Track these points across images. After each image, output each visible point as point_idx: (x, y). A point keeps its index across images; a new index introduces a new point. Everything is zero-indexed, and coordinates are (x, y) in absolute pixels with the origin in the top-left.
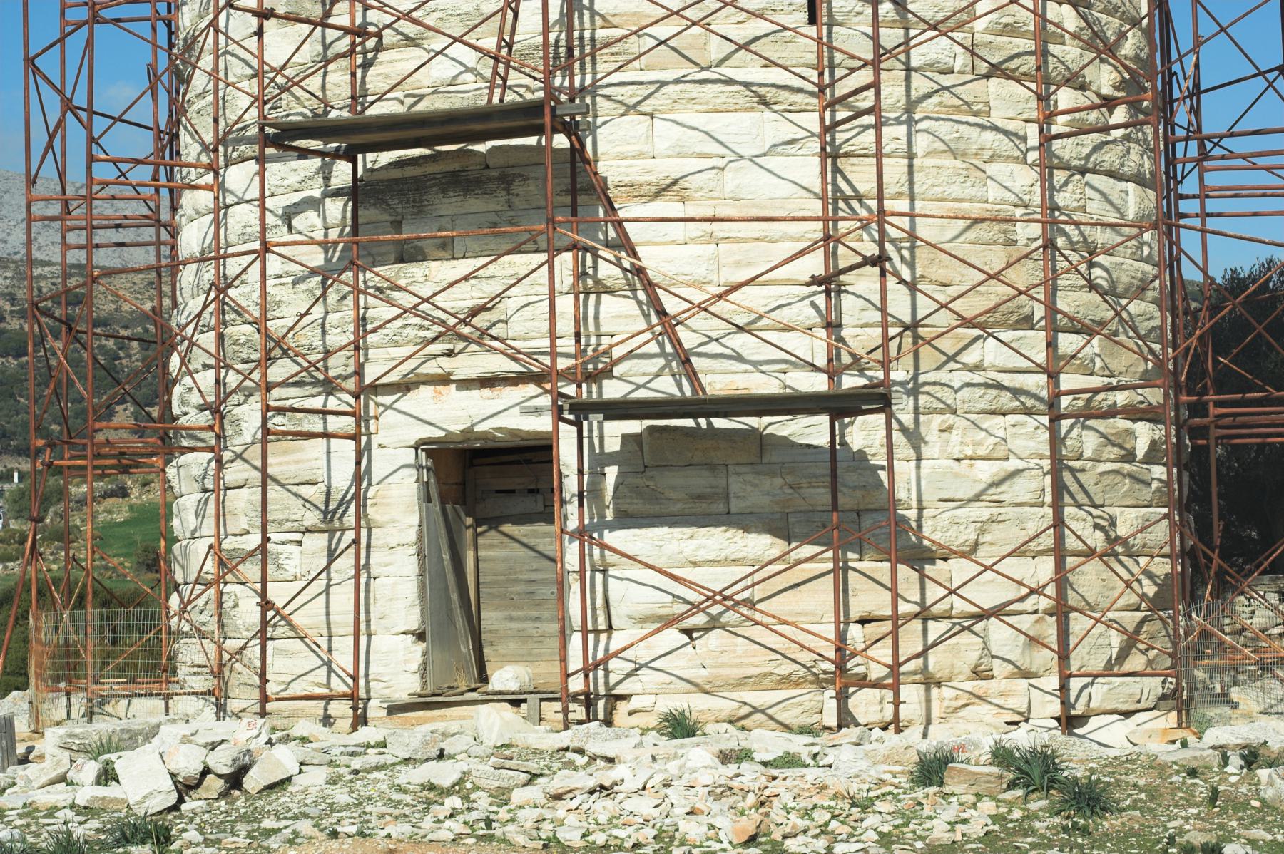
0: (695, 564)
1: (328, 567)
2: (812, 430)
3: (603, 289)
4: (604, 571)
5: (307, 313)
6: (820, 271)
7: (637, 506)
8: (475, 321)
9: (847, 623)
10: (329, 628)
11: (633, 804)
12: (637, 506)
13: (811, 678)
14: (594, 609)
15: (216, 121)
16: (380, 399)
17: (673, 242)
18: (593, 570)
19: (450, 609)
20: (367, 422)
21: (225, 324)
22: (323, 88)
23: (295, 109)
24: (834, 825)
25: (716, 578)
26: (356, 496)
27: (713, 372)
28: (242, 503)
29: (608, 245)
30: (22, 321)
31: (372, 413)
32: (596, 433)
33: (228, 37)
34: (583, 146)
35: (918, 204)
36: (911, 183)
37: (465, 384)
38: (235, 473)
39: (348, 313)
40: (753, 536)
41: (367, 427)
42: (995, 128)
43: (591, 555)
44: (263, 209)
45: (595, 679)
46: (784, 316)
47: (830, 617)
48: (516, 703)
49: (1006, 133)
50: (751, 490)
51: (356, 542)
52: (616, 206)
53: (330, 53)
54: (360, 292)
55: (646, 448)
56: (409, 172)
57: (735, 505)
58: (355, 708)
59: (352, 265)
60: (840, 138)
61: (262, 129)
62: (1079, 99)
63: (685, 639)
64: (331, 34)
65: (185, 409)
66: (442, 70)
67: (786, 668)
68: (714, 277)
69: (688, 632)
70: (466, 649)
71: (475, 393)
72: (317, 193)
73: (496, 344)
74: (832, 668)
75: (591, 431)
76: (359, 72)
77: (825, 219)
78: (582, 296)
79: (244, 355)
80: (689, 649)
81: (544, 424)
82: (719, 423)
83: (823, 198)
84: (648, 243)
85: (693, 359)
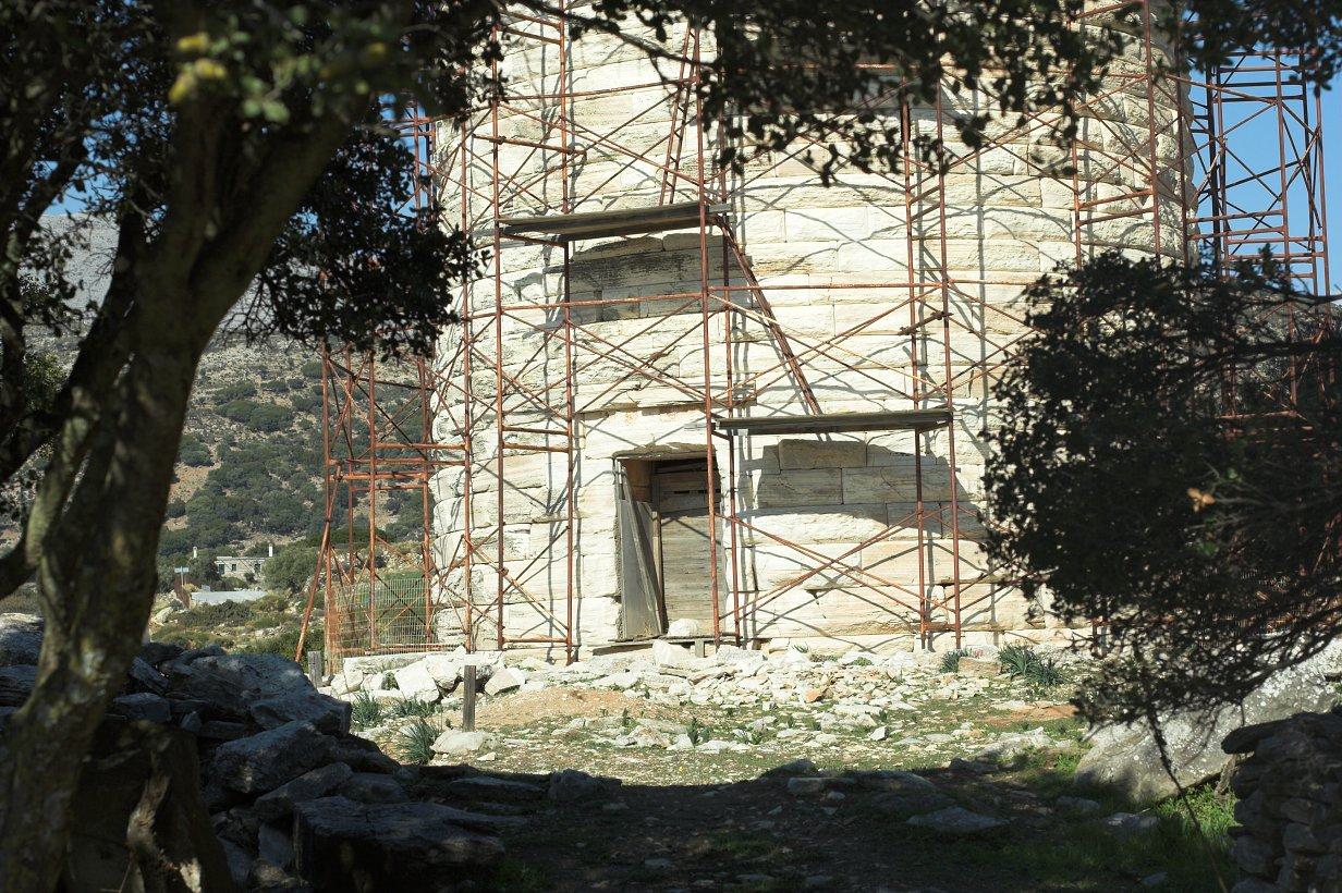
0: (818, 541)
1: (550, 547)
2: (901, 442)
3: (750, 340)
4: (752, 547)
5: (532, 360)
6: (907, 324)
7: (774, 499)
8: (656, 364)
9: (932, 585)
10: (551, 593)
11: (744, 684)
12: (774, 499)
13: (904, 625)
14: (744, 576)
15: (464, 216)
16: (587, 423)
17: (800, 304)
18: (744, 547)
19: (639, 581)
20: (577, 439)
21: (472, 369)
22: (544, 192)
23: (522, 210)
24: (876, 692)
25: (834, 550)
26: (569, 496)
27: (831, 400)
28: (485, 504)
29: (752, 308)
30: (273, 394)
31: (581, 433)
32: (745, 445)
33: (473, 154)
34: (733, 235)
35: (986, 274)
36: (981, 258)
37: (649, 410)
38: (479, 482)
39: (563, 359)
40: (860, 520)
41: (577, 443)
42: (1046, 216)
43: (741, 536)
44: (499, 281)
45: (745, 627)
46: (882, 358)
47: (917, 581)
48: (687, 645)
49: (1053, 219)
50: (860, 487)
51: (569, 528)
52: (757, 278)
53: (549, 166)
54: (571, 343)
55: (781, 456)
56: (607, 254)
57: (847, 498)
58: (569, 652)
59: (565, 323)
60: (925, 225)
61: (497, 225)
62: (1115, 191)
63: (811, 597)
64: (549, 153)
65: (442, 435)
66: (630, 178)
67: (886, 618)
68: (831, 330)
69: (813, 592)
70: (653, 609)
71: (656, 418)
72: (540, 271)
73: (670, 381)
74: (917, 616)
75: (741, 444)
76: (569, 180)
77: (911, 286)
78: (733, 345)
79: (486, 393)
80: (814, 604)
81: (699, 438)
82: (835, 437)
83: (910, 268)
84: (781, 305)
85: (814, 391)
